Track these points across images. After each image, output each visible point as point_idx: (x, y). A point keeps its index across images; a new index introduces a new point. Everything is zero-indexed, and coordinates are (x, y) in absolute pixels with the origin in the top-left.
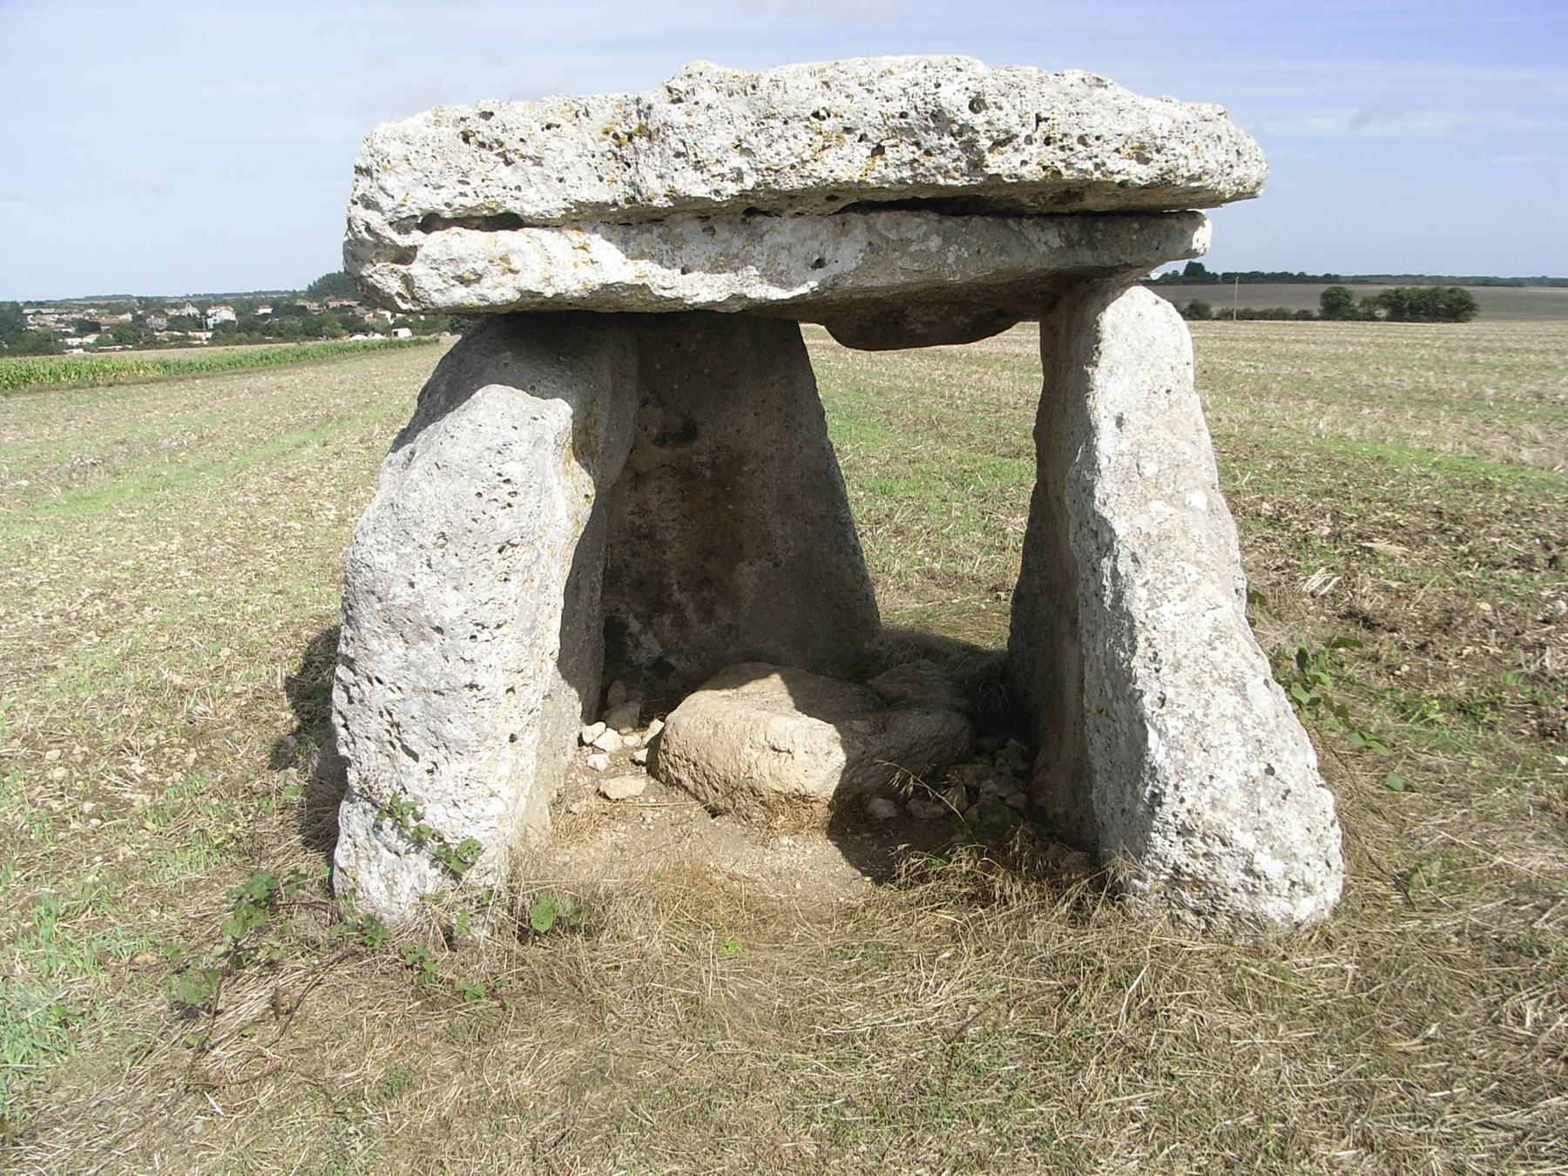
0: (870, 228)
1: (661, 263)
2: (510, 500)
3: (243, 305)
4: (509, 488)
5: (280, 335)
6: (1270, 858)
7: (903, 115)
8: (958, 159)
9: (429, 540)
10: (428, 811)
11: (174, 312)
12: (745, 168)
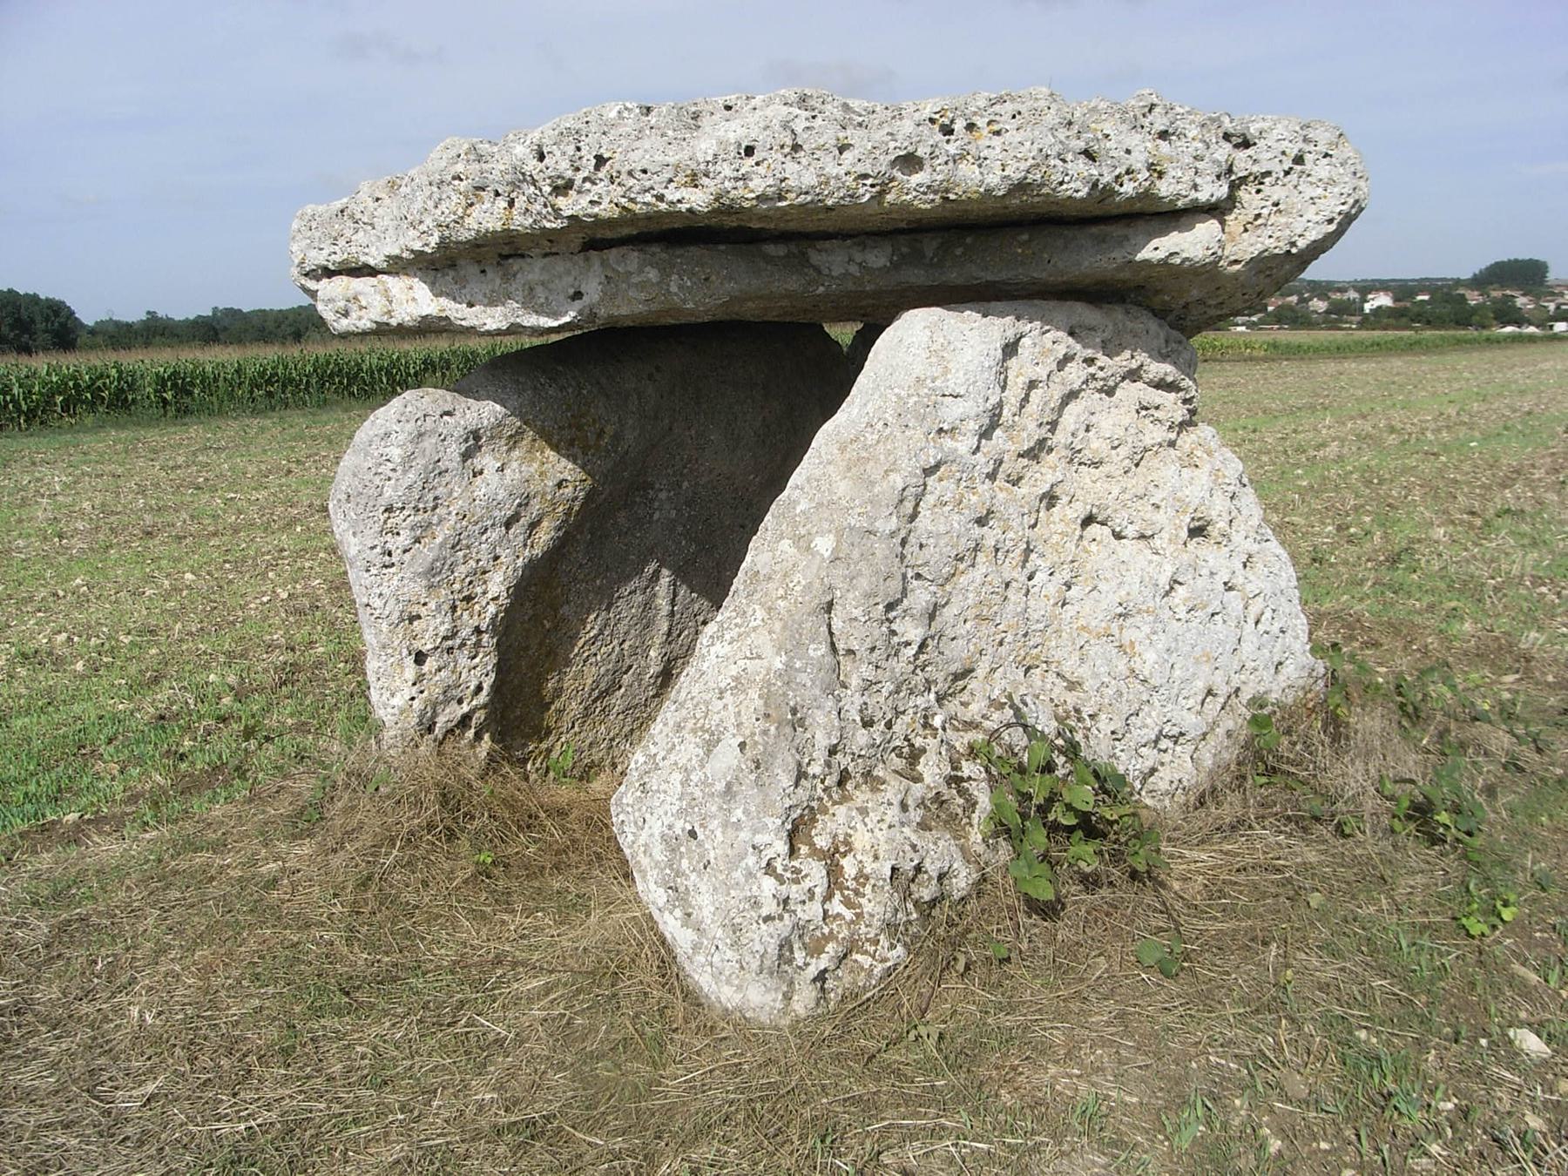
0: (604, 264)
1: (454, 299)
2: (391, 474)
3: (1403, 290)
4: (390, 466)
5: (1429, 323)
6: (679, 923)
11: (1337, 296)
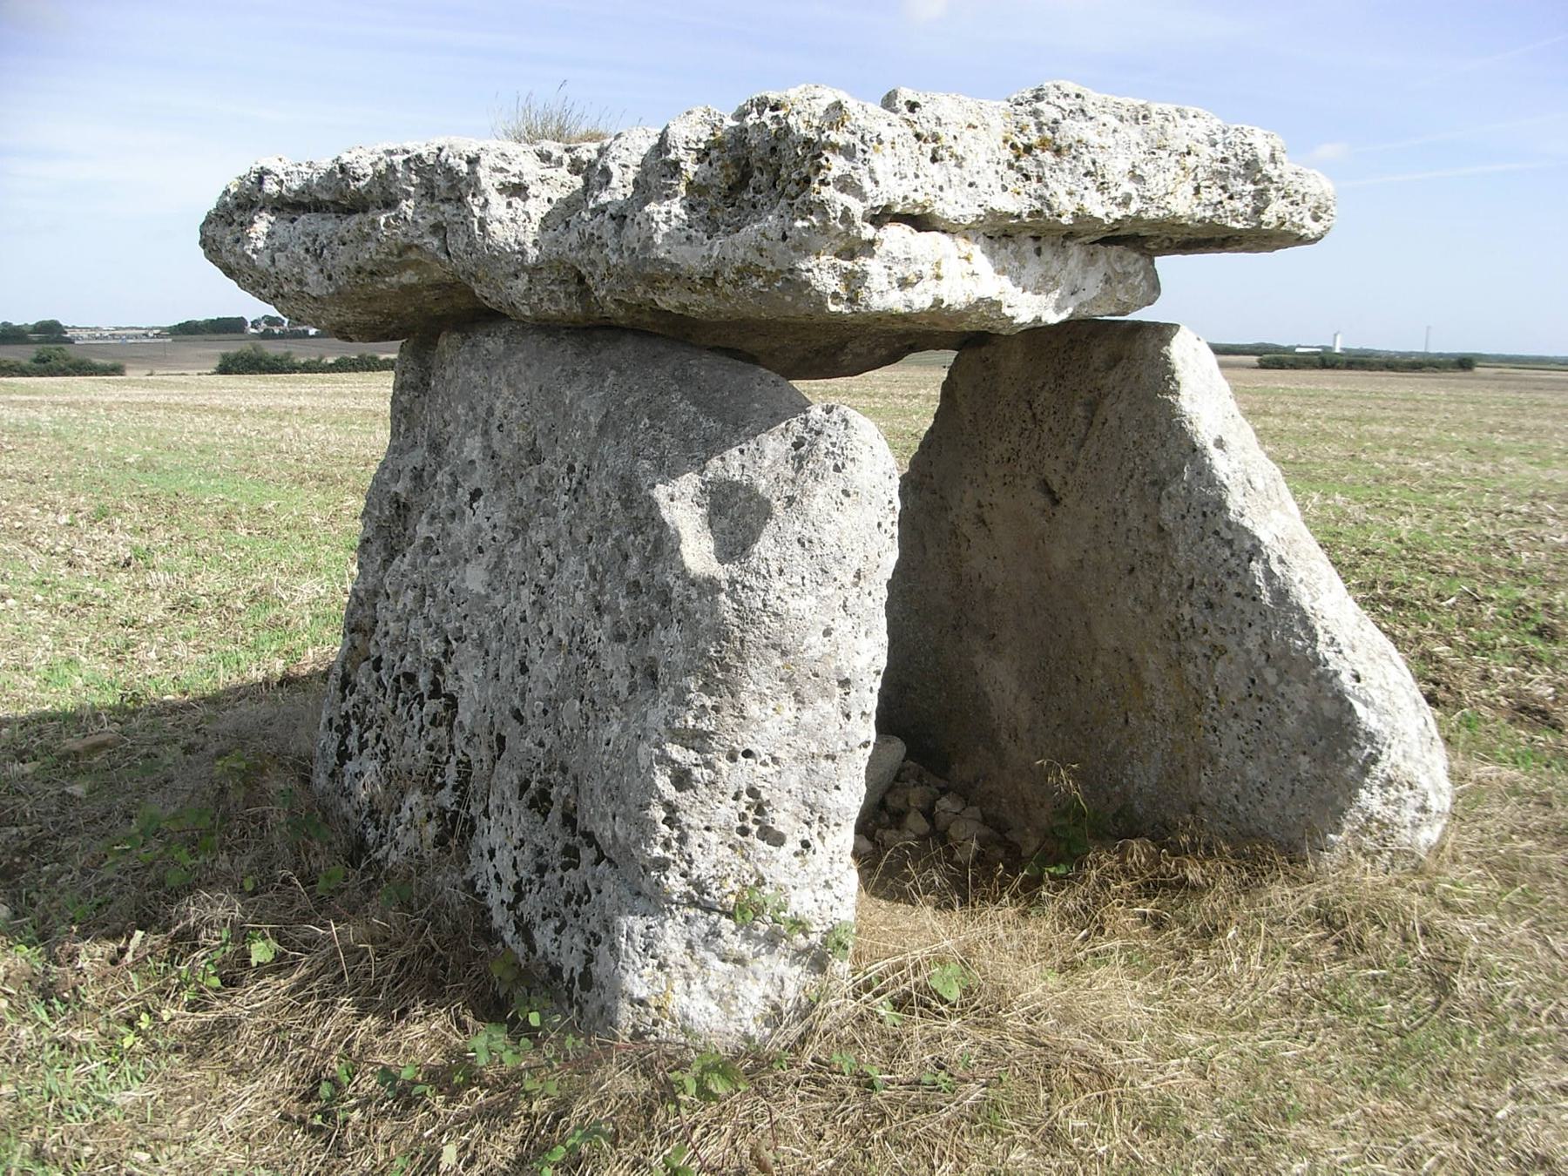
7: (1224, 160)
8: (1247, 205)
9: (848, 579)
10: (794, 900)
12: (1134, 194)
